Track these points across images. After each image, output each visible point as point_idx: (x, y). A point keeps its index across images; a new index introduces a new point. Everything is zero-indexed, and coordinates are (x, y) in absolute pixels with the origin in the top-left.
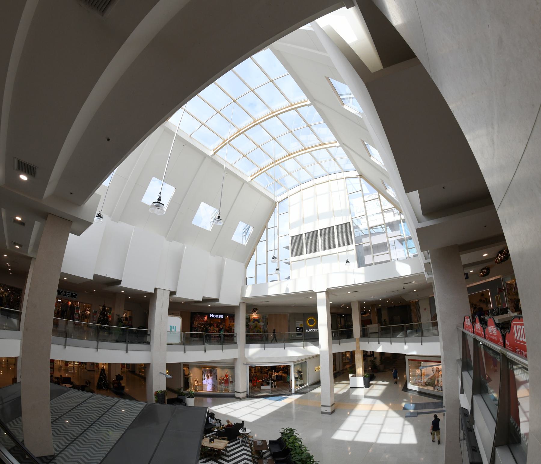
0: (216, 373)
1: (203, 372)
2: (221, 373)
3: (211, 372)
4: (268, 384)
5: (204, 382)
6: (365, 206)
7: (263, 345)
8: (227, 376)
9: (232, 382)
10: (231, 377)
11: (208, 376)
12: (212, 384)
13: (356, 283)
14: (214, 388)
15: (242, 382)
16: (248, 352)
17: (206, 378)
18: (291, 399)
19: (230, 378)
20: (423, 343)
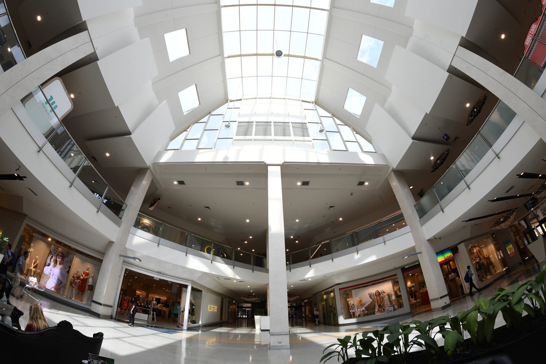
0: (71, 261)
1: (50, 253)
2: (79, 266)
3: (63, 256)
4: (145, 312)
5: (47, 270)
6: (109, 339)
7: (158, 238)
8: (87, 274)
9: (92, 288)
10: (93, 278)
11: (56, 262)
12: (58, 279)
13: (321, 161)
14: (60, 285)
15: (108, 289)
16: (132, 239)
17: (52, 264)
18: (183, 335)
19: (90, 280)
20: (444, 210)
